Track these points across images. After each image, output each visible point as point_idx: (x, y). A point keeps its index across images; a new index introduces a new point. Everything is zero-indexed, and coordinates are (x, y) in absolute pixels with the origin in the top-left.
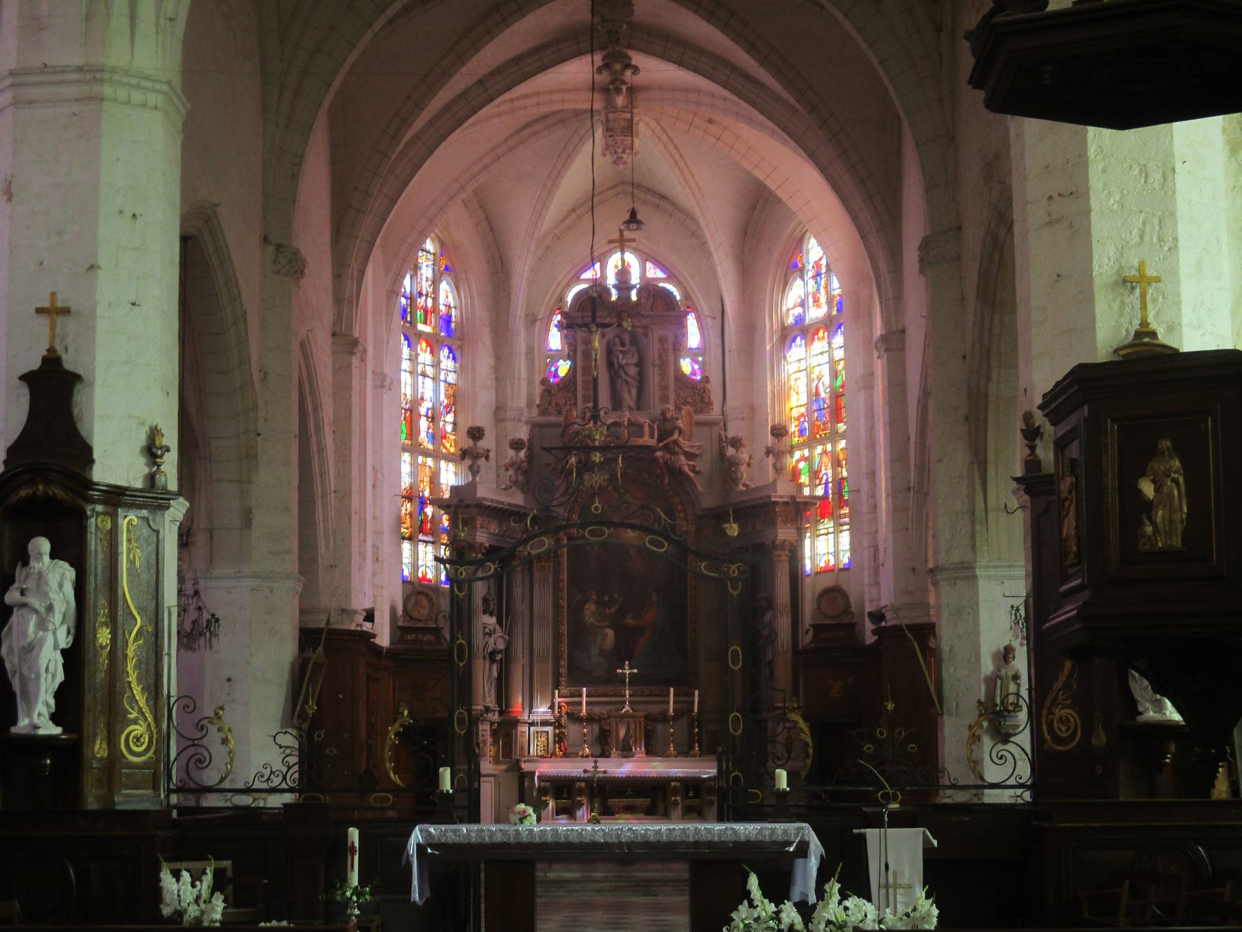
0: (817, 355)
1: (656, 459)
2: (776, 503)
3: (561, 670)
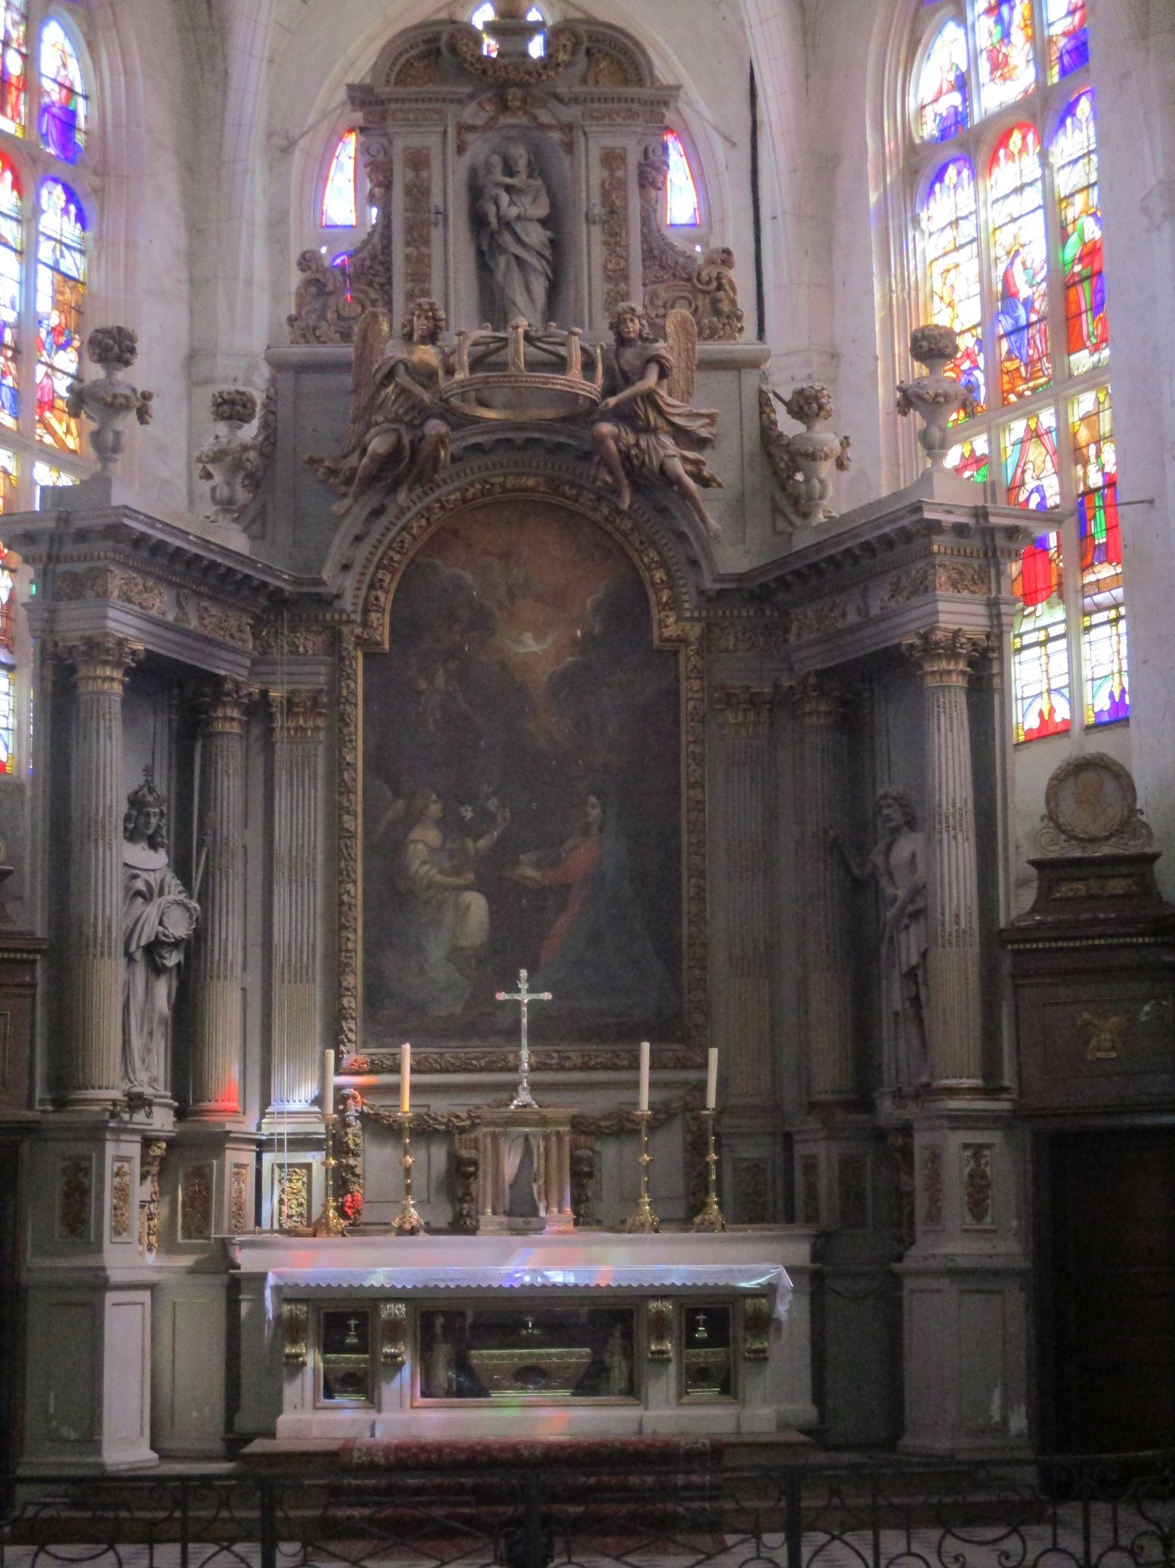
0: (1007, 196)
1: (600, 440)
2: (934, 527)
3: (345, 1002)
